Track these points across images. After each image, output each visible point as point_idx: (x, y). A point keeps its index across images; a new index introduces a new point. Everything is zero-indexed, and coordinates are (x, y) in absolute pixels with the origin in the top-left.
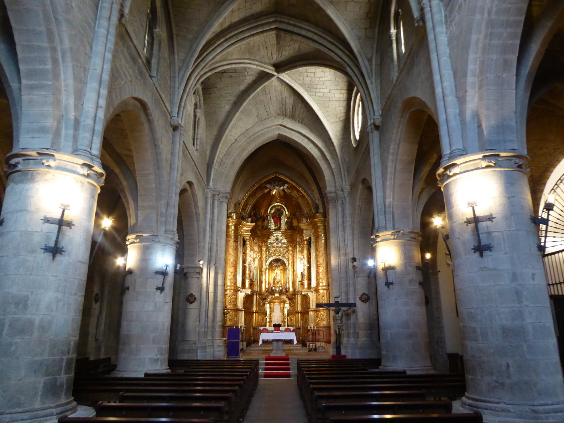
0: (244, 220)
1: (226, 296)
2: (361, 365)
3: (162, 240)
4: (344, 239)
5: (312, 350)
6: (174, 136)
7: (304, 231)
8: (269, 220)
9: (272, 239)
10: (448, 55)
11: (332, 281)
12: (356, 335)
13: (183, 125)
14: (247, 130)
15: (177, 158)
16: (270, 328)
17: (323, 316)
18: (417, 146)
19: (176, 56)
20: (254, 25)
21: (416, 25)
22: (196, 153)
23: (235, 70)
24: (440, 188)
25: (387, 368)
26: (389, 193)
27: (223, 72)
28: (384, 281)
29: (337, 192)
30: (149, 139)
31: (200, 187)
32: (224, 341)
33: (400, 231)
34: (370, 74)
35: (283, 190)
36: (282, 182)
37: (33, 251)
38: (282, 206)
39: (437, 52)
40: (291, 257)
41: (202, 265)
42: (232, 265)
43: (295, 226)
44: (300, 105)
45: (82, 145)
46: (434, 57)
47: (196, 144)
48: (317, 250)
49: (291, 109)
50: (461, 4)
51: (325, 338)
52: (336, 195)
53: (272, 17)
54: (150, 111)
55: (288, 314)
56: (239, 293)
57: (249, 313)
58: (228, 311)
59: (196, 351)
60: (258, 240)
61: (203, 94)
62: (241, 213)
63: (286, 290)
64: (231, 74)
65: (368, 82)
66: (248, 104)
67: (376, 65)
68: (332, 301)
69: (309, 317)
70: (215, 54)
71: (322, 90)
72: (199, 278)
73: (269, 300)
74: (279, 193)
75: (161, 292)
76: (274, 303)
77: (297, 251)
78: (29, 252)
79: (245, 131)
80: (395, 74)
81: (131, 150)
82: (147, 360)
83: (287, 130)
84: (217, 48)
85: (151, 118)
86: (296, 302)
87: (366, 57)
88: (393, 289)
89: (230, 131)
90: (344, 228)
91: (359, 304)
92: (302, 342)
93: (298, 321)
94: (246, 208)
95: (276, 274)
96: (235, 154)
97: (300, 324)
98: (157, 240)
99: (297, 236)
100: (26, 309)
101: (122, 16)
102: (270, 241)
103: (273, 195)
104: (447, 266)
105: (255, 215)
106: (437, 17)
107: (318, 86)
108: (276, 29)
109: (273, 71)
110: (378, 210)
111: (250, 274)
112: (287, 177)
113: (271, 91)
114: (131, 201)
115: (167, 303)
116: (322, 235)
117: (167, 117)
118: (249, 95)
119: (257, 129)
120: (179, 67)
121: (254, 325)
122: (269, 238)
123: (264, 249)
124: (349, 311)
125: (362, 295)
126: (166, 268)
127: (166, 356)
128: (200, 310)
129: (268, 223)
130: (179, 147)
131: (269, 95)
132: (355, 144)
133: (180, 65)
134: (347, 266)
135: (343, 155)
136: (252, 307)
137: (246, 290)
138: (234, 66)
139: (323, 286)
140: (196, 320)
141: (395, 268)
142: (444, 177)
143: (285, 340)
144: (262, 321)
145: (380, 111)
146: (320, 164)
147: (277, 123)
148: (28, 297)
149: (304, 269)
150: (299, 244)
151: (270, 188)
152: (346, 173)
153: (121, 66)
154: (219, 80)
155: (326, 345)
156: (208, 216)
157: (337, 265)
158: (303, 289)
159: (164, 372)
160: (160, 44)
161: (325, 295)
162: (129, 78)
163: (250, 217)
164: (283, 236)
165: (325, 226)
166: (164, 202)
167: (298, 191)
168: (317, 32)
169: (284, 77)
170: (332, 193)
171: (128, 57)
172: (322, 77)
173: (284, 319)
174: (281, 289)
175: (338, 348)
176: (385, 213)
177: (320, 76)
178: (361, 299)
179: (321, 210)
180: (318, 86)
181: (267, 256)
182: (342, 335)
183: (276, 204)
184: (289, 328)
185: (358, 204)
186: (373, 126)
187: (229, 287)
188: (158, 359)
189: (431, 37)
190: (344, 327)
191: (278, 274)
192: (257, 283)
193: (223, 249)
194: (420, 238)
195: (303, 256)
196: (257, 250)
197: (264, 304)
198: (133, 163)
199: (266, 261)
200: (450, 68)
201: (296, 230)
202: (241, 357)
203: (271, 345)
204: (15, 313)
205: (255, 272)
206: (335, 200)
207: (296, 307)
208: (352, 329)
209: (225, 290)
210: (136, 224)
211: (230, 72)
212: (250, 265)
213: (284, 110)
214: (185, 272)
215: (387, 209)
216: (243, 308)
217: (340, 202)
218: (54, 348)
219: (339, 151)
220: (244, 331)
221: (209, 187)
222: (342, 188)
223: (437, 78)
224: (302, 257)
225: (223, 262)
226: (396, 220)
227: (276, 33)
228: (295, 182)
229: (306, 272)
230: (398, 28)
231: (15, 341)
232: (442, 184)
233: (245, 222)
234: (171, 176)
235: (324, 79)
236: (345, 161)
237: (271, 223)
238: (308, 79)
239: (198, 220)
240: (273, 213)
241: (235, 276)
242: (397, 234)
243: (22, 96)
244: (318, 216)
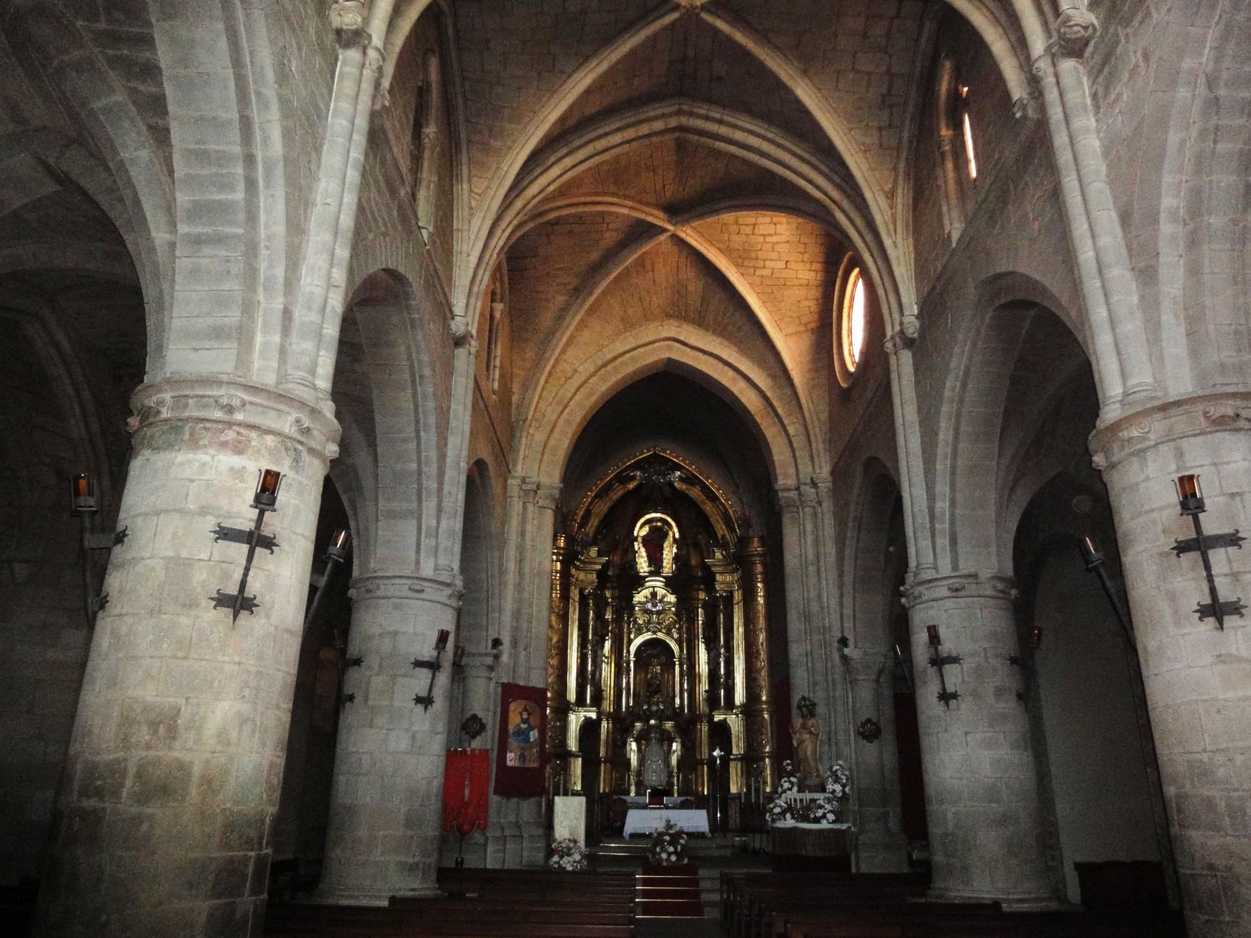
10: (1104, 178)
20: (632, 120)
21: (1018, 115)
23: (580, 219)
29: (802, 488)
37: (191, 605)
39: (1078, 171)
45: (298, 368)
46: (1070, 183)
50: (1137, 66)
52: (800, 494)
65: (888, 242)
71: (768, 264)
75: (426, 708)
78: (184, 606)
83: (688, 350)
99: (698, 589)
100: (174, 738)
106: (1073, 97)
125: (863, 725)
131: (651, 274)
138: (580, 209)
145: (915, 307)
147: (665, 335)
148: (180, 709)
154: (544, 240)
162: (383, 229)
170: (789, 490)
172: (770, 235)
176: (933, 536)
188: (417, 864)
189: (1060, 139)
197: (624, 744)
200: (1111, 205)
204: (148, 747)
212: (932, 607)
218: (232, 832)
223: (1080, 228)
231: (149, 811)
235: (775, 239)
238: (735, 238)
243: (177, 261)
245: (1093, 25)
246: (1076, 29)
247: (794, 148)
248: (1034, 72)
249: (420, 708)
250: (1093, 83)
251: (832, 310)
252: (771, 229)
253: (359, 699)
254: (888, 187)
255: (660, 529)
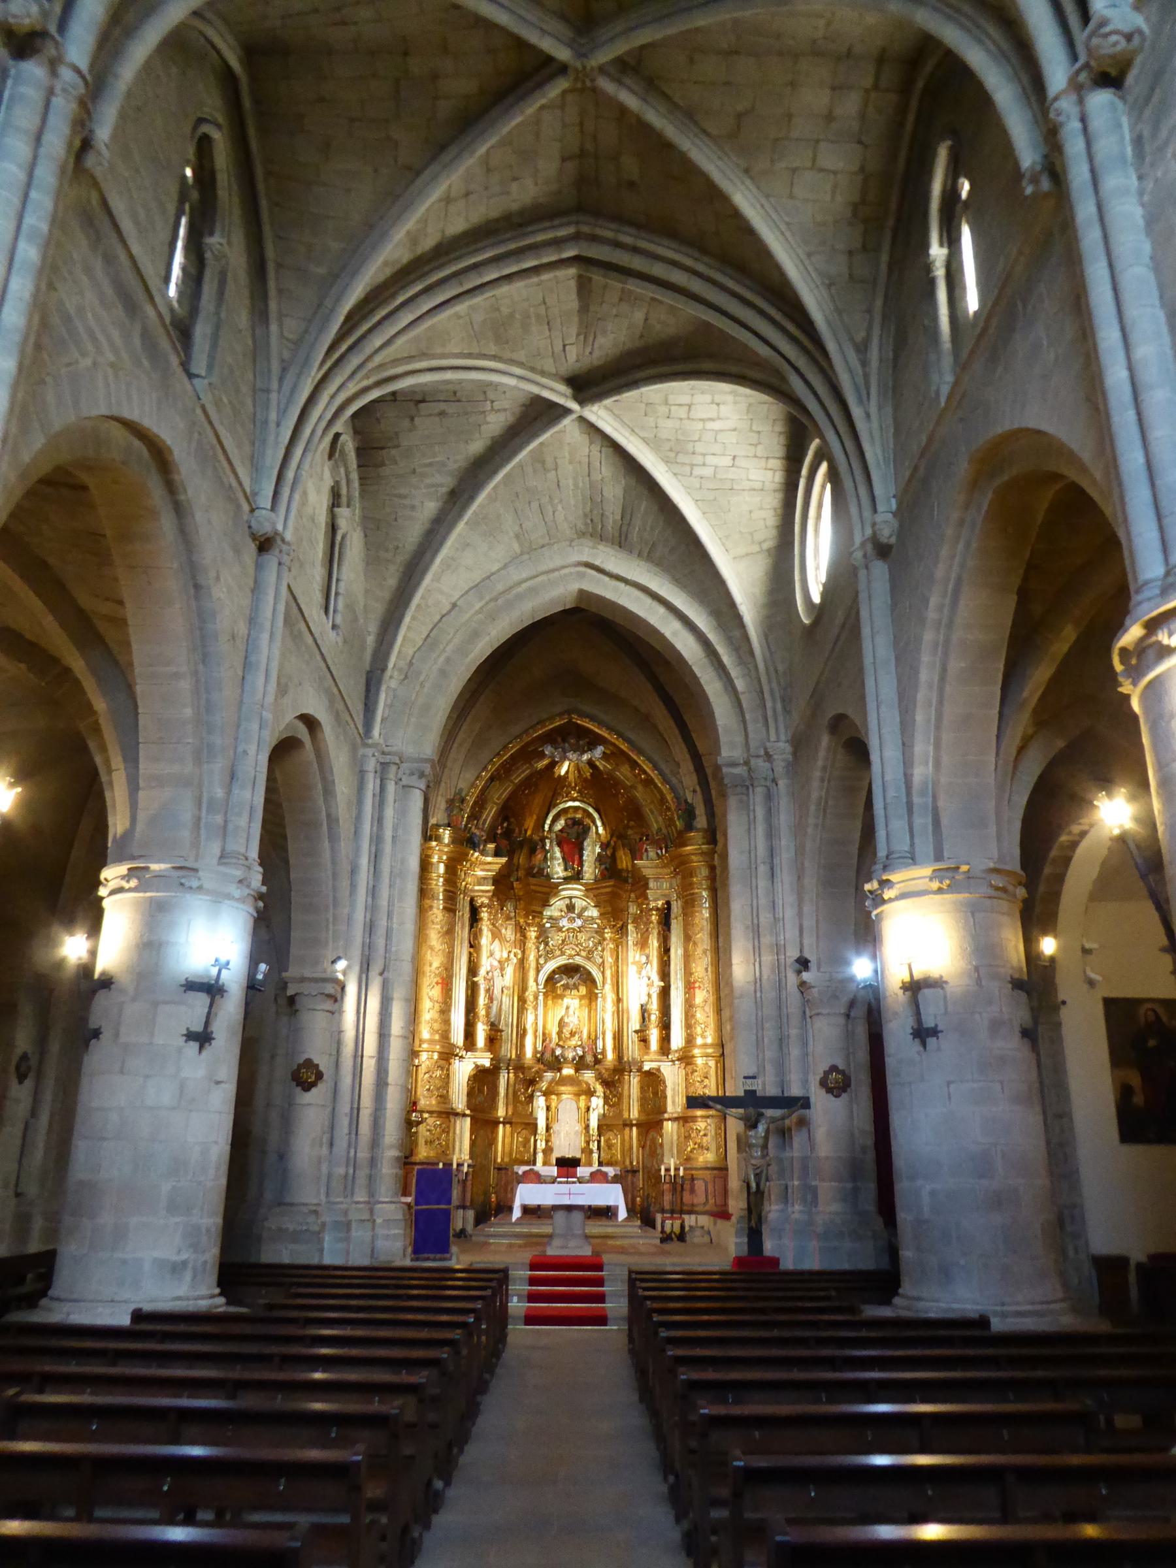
0: (474, 846)
1: (417, 1070)
2: (833, 1293)
3: (207, 885)
4: (774, 902)
5: (672, 1239)
6: (259, 567)
7: (651, 884)
8: (547, 852)
9: (556, 907)
10: (1147, 260)
11: (733, 1029)
12: (810, 1196)
13: (288, 536)
14: (488, 577)
15: (265, 636)
16: (546, 1168)
17: (705, 1135)
18: (1015, 597)
19: (274, 328)
20: (512, 246)
21: (1029, 190)
22: (332, 635)
24: (1127, 698)
25: (921, 1305)
26: (922, 747)
27: (419, 398)
28: (909, 1023)
29: (753, 761)
30: (175, 565)
31: (342, 738)
32: (406, 1207)
33: (958, 868)
34: (864, 393)
35: (590, 763)
36: (587, 740)
38: (585, 811)
40: (610, 960)
41: (344, 973)
42: (435, 980)
43: (622, 870)
44: (644, 505)
47: (335, 611)
48: (688, 938)
49: (619, 517)
51: (711, 1201)
52: (750, 770)
53: (569, 224)
54: (179, 473)
55: (599, 1127)
56: (457, 1061)
57: (484, 1123)
58: (421, 1117)
59: (317, 1237)
60: (515, 908)
61: (359, 466)
62: (466, 826)
63: (595, 1056)
64: (443, 406)
65: (857, 412)
66: (492, 499)
67: (881, 361)
68: (735, 1089)
69: (661, 1136)
70: (393, 332)
71: (710, 460)
72: (333, 1013)
73: (544, 1085)
74: (579, 772)
75: (201, 1048)
76: (558, 1094)
77: (630, 943)
79: (483, 580)
80: (944, 379)
81: (120, 603)
82: (147, 1266)
83: (607, 579)
84: (401, 314)
85: (182, 497)
86: (626, 1093)
87: (852, 339)
88: (939, 1049)
89: (437, 579)
90: (772, 869)
91: (821, 1102)
92: (643, 1214)
93: (631, 1148)
94: (481, 813)
95: (568, 1008)
96: (449, 648)
97: (637, 1157)
98: (195, 884)
101: (84, 146)
102: (549, 913)
103: (560, 776)
104: (1086, 986)
105: (508, 833)
106: (1106, 146)
107: (700, 448)
108: (577, 259)
109: (566, 396)
110: (888, 801)
111: (488, 1008)
112: (601, 724)
113: (559, 462)
114: (117, 761)
115: (218, 1083)
116: (705, 894)
117: (239, 507)
118: (495, 472)
119: (516, 574)
120: (283, 361)
121: (499, 1160)
122: (546, 904)
123: (532, 933)
124: (787, 1122)
125: (826, 1073)
126: (220, 971)
127: (212, 1254)
128: (334, 1109)
129: (545, 858)
130: (275, 604)
132: (808, 616)
133: (286, 355)
134: (780, 986)
135: (771, 653)
136: (493, 1105)
137: (477, 1054)
139: (705, 1046)
140: (321, 1140)
141: (946, 982)
142: (880, 901)
143: (590, 1207)
144: (524, 1146)
146: (702, 681)
149: (649, 996)
150: (636, 920)
151: (553, 756)
152: (779, 706)
153: (81, 310)
154: (406, 423)
155: (715, 1224)
156: (367, 827)
157: (751, 979)
158: (647, 1053)
159: (203, 1305)
160: (222, 283)
161: (713, 1072)
162: (111, 357)
163: (492, 837)
164: (587, 897)
165: (712, 868)
166: (218, 767)
167: (634, 764)
168: (701, 268)
169: (599, 417)
171: (109, 291)
173: (588, 1143)
174: (580, 1053)
175: (754, 1236)
177: (704, 416)
178: (823, 1083)
179: (701, 821)
180: (700, 448)
181: (540, 956)
182: (766, 1194)
183: (570, 804)
184: (604, 1169)
185: (815, 795)
186: (869, 547)
187: (425, 1046)
188: (184, 1263)
190: (773, 1169)
191: (571, 1011)
192: (509, 1034)
193: (410, 926)
194: (1021, 892)
195: (648, 957)
196: (513, 938)
197: (530, 1098)
198: (128, 644)
199: (538, 971)
201: (626, 881)
202: (454, 1258)
203: (549, 1222)
205: (506, 1001)
206: (746, 785)
207: (625, 1106)
208: (796, 1176)
209: (414, 1054)
210: (128, 834)
211: (439, 401)
212: (490, 980)
213: (597, 520)
214: (290, 992)
215: (916, 800)
216: (468, 1108)
217: (760, 791)
219: (760, 643)
220: (470, 1177)
221: (370, 741)
222: (766, 749)
223: (1108, 336)
224: (644, 959)
225: (407, 967)
226: (944, 829)
227: (580, 277)
228: (627, 740)
229: (654, 1006)
230: (952, 240)
232: (1135, 684)
233: (477, 854)
234: (247, 688)
235: (716, 425)
236: (776, 672)
237: (553, 858)
238: (669, 424)
239: (333, 838)
240: (561, 831)
241: (445, 1011)
242: (950, 874)
244: (691, 838)
245: (1139, 31)
246: (1114, 38)
247: (731, 284)
248: (1052, 115)
249: (194, 1046)
250: (1136, 124)
251: (793, 523)
252: (712, 412)
253: (106, 1036)
254: (860, 336)
255: (575, 823)
